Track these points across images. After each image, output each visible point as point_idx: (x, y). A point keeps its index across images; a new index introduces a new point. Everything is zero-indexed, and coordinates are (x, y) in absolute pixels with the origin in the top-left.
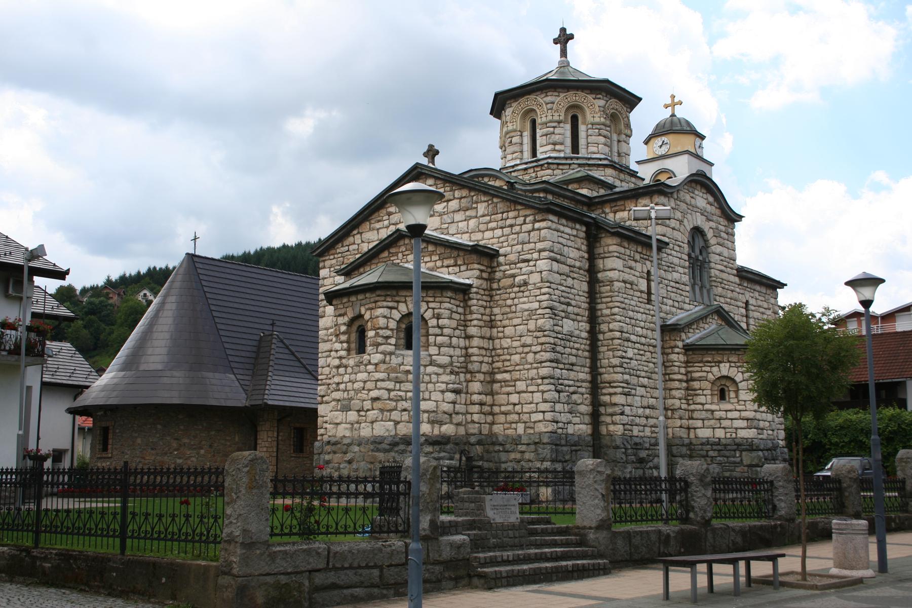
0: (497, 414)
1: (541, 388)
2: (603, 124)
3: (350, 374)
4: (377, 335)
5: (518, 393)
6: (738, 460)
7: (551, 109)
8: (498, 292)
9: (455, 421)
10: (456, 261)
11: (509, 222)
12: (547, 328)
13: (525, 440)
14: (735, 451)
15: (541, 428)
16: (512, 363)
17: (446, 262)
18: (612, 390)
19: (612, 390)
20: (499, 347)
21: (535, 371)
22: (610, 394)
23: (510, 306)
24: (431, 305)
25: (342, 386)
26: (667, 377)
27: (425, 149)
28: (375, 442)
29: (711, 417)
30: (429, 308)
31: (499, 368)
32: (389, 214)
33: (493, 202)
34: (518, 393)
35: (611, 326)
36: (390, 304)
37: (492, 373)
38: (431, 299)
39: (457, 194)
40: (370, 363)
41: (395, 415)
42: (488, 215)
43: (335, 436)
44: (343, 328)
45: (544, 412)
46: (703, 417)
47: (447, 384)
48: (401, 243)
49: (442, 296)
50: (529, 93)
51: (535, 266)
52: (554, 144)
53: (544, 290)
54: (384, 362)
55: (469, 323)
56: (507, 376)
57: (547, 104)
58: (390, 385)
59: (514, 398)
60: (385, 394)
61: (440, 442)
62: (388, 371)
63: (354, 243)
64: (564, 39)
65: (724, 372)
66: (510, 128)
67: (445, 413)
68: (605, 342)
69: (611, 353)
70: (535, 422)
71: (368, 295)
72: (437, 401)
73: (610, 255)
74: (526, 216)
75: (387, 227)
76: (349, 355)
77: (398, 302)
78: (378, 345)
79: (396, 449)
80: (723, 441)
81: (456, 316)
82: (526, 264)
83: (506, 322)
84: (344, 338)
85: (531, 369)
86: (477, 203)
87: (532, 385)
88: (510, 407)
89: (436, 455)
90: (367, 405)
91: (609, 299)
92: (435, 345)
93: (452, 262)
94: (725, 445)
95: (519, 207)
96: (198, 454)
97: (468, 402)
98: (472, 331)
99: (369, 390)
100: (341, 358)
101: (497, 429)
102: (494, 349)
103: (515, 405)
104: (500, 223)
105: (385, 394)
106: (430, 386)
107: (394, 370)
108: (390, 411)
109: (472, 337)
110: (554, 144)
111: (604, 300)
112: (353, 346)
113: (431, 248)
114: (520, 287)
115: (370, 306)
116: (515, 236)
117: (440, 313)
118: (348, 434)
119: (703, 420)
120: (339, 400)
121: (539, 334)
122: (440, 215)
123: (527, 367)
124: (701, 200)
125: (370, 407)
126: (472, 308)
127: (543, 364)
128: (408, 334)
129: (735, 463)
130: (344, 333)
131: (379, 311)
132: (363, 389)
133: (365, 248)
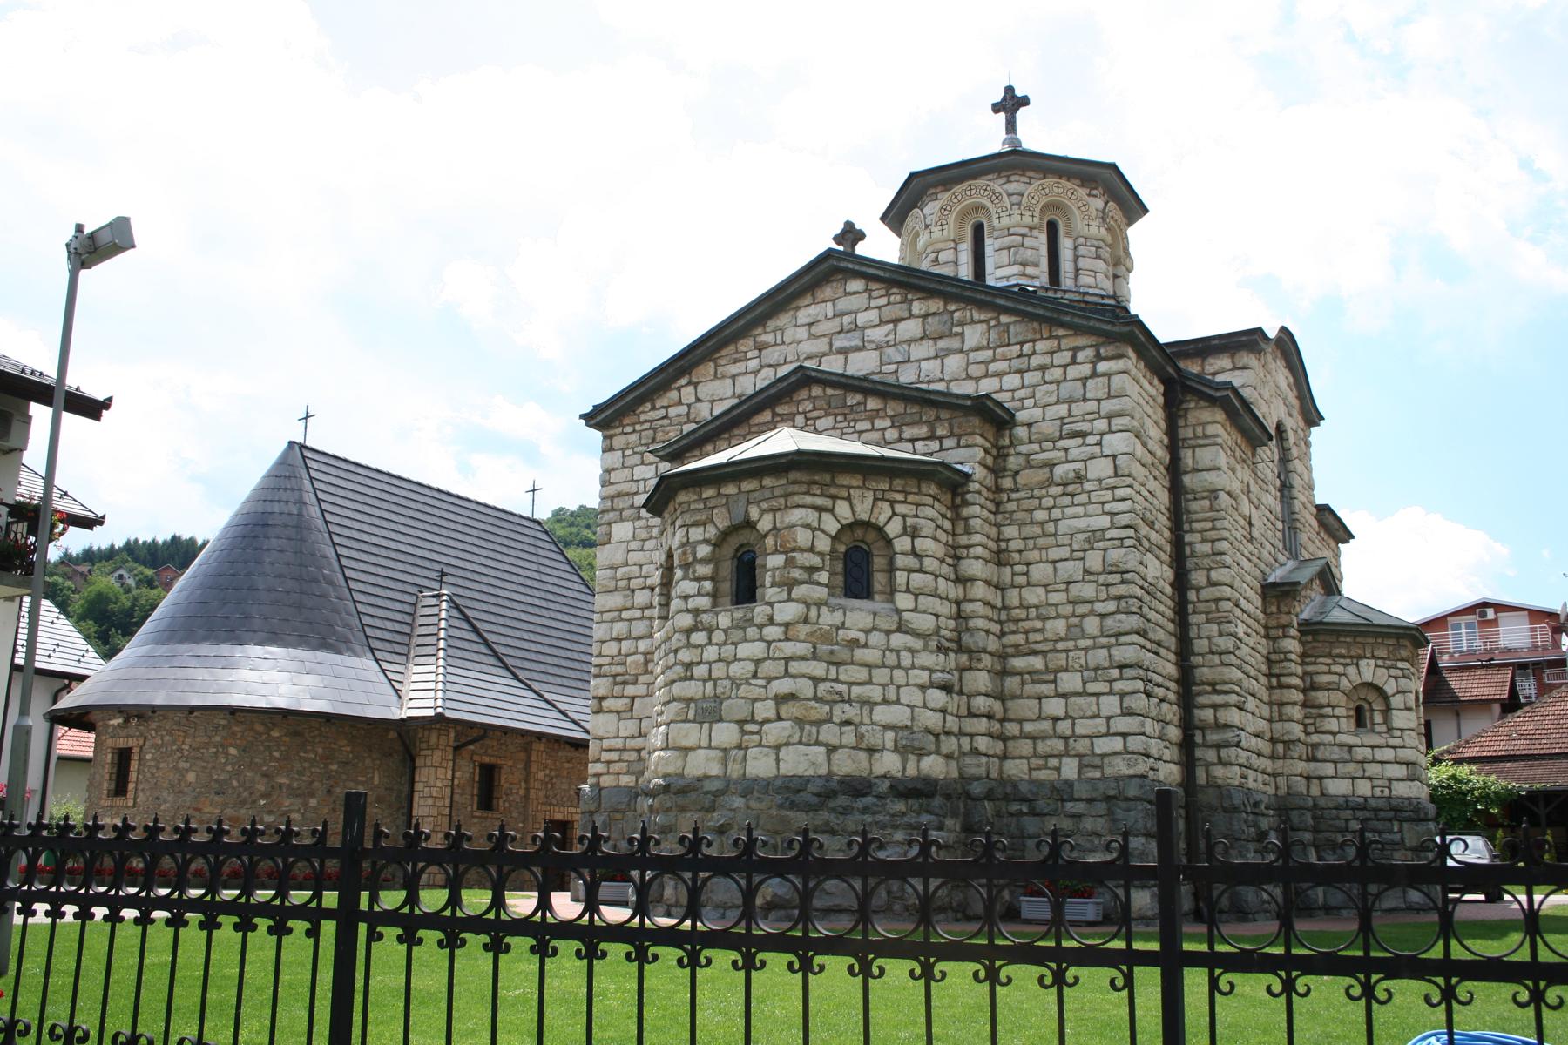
0: (1014, 738)
1: (1118, 686)
4: (790, 563)
5: (1064, 696)
6: (1397, 837)
8: (1014, 496)
9: (944, 749)
10: (933, 430)
12: (1129, 566)
13: (1081, 791)
14: (1390, 820)
15: (1121, 767)
16: (1049, 635)
17: (908, 432)
20: (1016, 602)
21: (1104, 652)
22: (1215, 707)
23: (1042, 523)
24: (900, 508)
25: (700, 671)
26: (1274, 681)
27: (838, 229)
29: (1347, 757)
30: (894, 514)
31: (1017, 646)
32: (761, 348)
33: (999, 324)
34: (1064, 696)
35: (1214, 575)
36: (820, 501)
37: (1002, 656)
38: (900, 497)
39: (917, 308)
40: (771, 621)
41: (829, 733)
42: (989, 348)
43: (682, 776)
45: (1124, 735)
46: (1335, 757)
47: (932, 671)
48: (803, 394)
52: (1024, 264)
53: (1120, 493)
54: (806, 621)
56: (1037, 662)
57: (1009, 195)
58: (818, 669)
59: (1055, 707)
60: (806, 688)
61: (917, 791)
63: (680, 403)
64: (1011, 104)
65: (1368, 677)
67: (928, 731)
68: (1201, 607)
69: (1215, 627)
70: (1103, 756)
71: (768, 482)
72: (912, 707)
73: (1210, 441)
74: (1075, 350)
75: (756, 373)
77: (834, 498)
78: (790, 584)
79: (832, 804)
80: (1373, 803)
81: (942, 536)
82: (1080, 441)
83: (1034, 555)
84: (704, 570)
85: (1094, 647)
86: (962, 324)
87: (1096, 680)
88: (1046, 725)
89: (911, 819)
90: (765, 710)
91: (1209, 525)
92: (908, 591)
93: (923, 430)
94: (1376, 810)
95: (1061, 332)
96: (305, 804)
97: (964, 711)
98: (973, 567)
99: (770, 679)
100: (696, 612)
101: (1016, 769)
102: (1004, 608)
103: (1056, 719)
104: (1016, 364)
105: (806, 688)
107: (826, 638)
108: (818, 723)
109: (972, 580)
110: (1024, 264)
111: (1196, 526)
113: (873, 403)
116: (1054, 387)
117: (911, 525)
118: (715, 770)
119: (1335, 762)
120: (691, 699)
122: (879, 348)
123: (1082, 643)
124: (1282, 377)
127: (1123, 639)
129: (1393, 843)
131: (796, 515)
132: (755, 676)
133: (704, 412)
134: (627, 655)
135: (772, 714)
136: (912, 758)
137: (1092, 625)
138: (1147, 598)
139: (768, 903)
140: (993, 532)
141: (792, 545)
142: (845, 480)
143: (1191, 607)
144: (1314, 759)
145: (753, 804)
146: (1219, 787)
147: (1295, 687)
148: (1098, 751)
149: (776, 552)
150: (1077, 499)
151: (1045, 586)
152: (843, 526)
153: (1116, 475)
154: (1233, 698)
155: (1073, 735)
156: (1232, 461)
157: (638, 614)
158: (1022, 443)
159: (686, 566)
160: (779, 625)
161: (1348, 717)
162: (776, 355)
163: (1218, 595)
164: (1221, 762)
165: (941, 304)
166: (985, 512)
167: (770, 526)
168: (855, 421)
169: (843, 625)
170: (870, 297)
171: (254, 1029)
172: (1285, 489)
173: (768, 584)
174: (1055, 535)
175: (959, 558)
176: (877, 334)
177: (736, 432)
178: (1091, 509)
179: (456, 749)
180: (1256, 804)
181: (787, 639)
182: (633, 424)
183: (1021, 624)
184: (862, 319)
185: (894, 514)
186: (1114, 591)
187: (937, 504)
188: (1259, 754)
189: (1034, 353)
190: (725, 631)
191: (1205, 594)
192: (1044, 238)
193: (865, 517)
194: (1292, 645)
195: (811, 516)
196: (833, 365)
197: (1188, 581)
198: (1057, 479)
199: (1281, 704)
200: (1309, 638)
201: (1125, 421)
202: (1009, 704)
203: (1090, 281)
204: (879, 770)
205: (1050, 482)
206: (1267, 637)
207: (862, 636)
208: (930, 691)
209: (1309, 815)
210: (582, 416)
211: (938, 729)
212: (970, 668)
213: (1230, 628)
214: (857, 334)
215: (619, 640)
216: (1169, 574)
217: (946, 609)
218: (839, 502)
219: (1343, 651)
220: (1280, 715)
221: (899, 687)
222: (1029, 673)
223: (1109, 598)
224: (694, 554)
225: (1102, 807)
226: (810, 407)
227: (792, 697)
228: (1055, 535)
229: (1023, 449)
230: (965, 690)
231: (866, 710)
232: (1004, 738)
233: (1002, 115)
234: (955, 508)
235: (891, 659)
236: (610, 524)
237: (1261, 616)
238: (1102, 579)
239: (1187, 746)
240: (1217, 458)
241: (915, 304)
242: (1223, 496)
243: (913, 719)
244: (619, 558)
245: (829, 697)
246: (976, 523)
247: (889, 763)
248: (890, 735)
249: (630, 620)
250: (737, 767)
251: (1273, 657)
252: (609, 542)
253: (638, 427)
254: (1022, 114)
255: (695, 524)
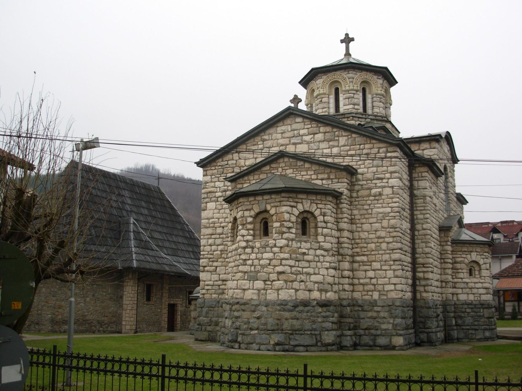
0: (356, 285)
1: (393, 267)
2: (382, 95)
3: (256, 253)
4: (282, 226)
5: (374, 270)
6: (482, 314)
7: (352, 82)
8: (357, 199)
9: (334, 290)
10: (329, 176)
11: (365, 151)
12: (397, 226)
13: (379, 303)
14: (480, 308)
15: (393, 295)
16: (369, 249)
17: (320, 176)
18: (424, 269)
19: (424, 269)
21: (388, 256)
22: (424, 272)
23: (367, 210)
24: (320, 206)
25: (249, 262)
26: (442, 261)
27: (292, 97)
28: (282, 304)
30: (317, 208)
31: (357, 253)
32: (264, 140)
33: (352, 137)
35: (425, 226)
37: (352, 256)
39: (322, 129)
40: (275, 246)
41: (296, 285)
42: (348, 145)
44: (250, 220)
45: (395, 284)
46: (462, 287)
47: (330, 263)
48: (281, 160)
49: (326, 200)
50: (336, 70)
51: (387, 182)
52: (354, 105)
53: (394, 200)
54: (287, 246)
55: (340, 220)
56: (365, 258)
58: (292, 263)
59: (371, 274)
61: (324, 304)
62: (291, 253)
63: (233, 159)
64: (347, 40)
65: (474, 259)
66: (322, 92)
67: (329, 284)
68: (420, 237)
69: (424, 244)
70: (388, 291)
71: (273, 196)
72: (323, 276)
73: (423, 178)
74: (379, 148)
76: (254, 239)
78: (283, 233)
79: (297, 309)
80: (474, 302)
81: (333, 215)
82: (380, 181)
84: (250, 226)
85: (385, 254)
86: (338, 136)
88: (368, 280)
89: (323, 314)
90: (273, 276)
91: (423, 208)
92: (322, 235)
93: (326, 176)
94: (475, 305)
95: (374, 141)
99: (275, 266)
100: (247, 241)
101: (357, 295)
102: (353, 239)
103: (371, 278)
104: (358, 152)
105: (287, 269)
106: (319, 264)
107: (294, 252)
108: (292, 281)
109: (343, 230)
110: (354, 105)
112: (258, 232)
113: (307, 165)
114: (375, 196)
115: (276, 204)
117: (323, 211)
118: (255, 297)
119: (462, 289)
120: (246, 272)
121: (391, 230)
123: (380, 252)
124: (446, 148)
125: (276, 278)
126: (343, 210)
127: (395, 251)
128: (305, 224)
129: (480, 316)
130: (250, 223)
131: (284, 209)
134: (214, 251)
135: (276, 278)
136: (324, 293)
137: (384, 246)
138: (403, 236)
139: (276, 343)
140: (350, 212)
141: (283, 219)
142: (300, 196)
143: (416, 237)
144: (455, 287)
145: (270, 309)
146: (424, 300)
147: (450, 263)
148: (385, 290)
149: (277, 221)
150: (380, 202)
151: (368, 232)
152: (300, 212)
153: (393, 194)
154: (430, 269)
155: (377, 284)
156: (431, 185)
157: (218, 236)
158: (360, 181)
159: (243, 225)
160: (278, 247)
161: (467, 272)
162: (269, 144)
163: (426, 233)
164: (426, 291)
165: (331, 128)
166: (348, 206)
167: (274, 212)
168: (301, 171)
169: (300, 248)
170: (305, 124)
171: (94, 389)
172: (447, 187)
173: (274, 233)
174: (371, 214)
175: (339, 222)
176: (307, 138)
177: (256, 173)
178: (384, 205)
179: (138, 279)
180: (436, 305)
181: (281, 253)
182: (215, 166)
183: (359, 245)
184: (302, 132)
185: (317, 208)
186: (392, 234)
187: (332, 204)
188: (437, 287)
189: (364, 149)
190: (258, 249)
191: (421, 232)
192: (361, 94)
193: (307, 209)
194: (449, 248)
195: (288, 209)
196: (291, 149)
197: (415, 228)
198: (372, 194)
199: (445, 269)
200: (454, 245)
201: (397, 175)
202: (355, 273)
203: (378, 110)
204: (312, 297)
205: (370, 195)
206: (440, 245)
207: (306, 251)
208: (329, 270)
209: (453, 307)
210: (195, 163)
211: (332, 283)
212: (342, 261)
213: (430, 245)
214: (300, 138)
215: (211, 245)
216: (409, 225)
217: (334, 240)
218: (299, 204)
219: (466, 250)
220: (444, 273)
221: (319, 269)
222: (362, 262)
223: (390, 237)
224: (246, 221)
225: (387, 308)
226: (284, 165)
227: (283, 273)
228: (371, 214)
229: (361, 183)
230: (340, 269)
231: (308, 277)
232: (353, 285)
233: (344, 44)
234: (337, 204)
235: (317, 259)
236: (206, 203)
237: (439, 238)
238: (388, 230)
239: (414, 286)
240: (426, 183)
241: (321, 128)
242: (428, 198)
243: (324, 280)
244: (210, 215)
245: (296, 273)
246: (344, 210)
247: (316, 295)
248: (316, 285)
249: (215, 239)
250: (263, 296)
251: (442, 252)
252: (206, 210)
253: (217, 167)
254: (351, 44)
255: (246, 210)
